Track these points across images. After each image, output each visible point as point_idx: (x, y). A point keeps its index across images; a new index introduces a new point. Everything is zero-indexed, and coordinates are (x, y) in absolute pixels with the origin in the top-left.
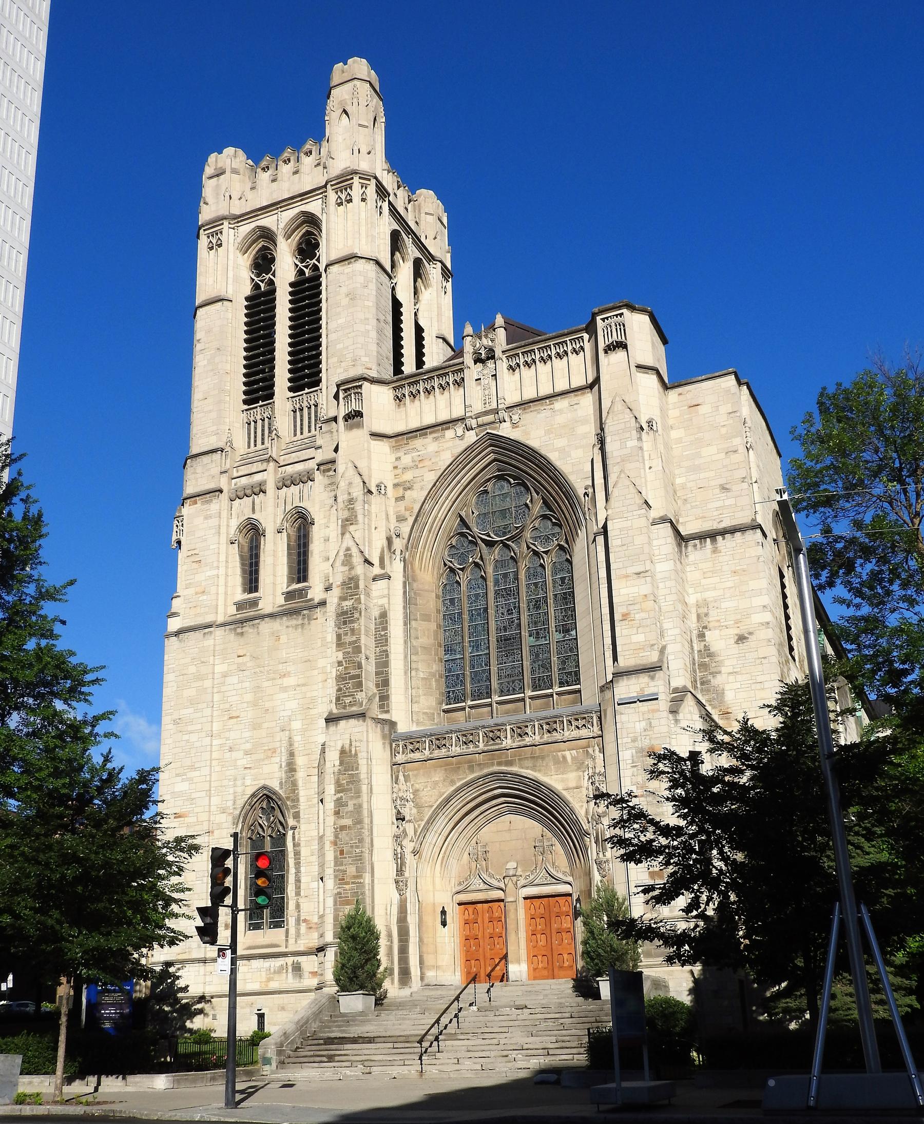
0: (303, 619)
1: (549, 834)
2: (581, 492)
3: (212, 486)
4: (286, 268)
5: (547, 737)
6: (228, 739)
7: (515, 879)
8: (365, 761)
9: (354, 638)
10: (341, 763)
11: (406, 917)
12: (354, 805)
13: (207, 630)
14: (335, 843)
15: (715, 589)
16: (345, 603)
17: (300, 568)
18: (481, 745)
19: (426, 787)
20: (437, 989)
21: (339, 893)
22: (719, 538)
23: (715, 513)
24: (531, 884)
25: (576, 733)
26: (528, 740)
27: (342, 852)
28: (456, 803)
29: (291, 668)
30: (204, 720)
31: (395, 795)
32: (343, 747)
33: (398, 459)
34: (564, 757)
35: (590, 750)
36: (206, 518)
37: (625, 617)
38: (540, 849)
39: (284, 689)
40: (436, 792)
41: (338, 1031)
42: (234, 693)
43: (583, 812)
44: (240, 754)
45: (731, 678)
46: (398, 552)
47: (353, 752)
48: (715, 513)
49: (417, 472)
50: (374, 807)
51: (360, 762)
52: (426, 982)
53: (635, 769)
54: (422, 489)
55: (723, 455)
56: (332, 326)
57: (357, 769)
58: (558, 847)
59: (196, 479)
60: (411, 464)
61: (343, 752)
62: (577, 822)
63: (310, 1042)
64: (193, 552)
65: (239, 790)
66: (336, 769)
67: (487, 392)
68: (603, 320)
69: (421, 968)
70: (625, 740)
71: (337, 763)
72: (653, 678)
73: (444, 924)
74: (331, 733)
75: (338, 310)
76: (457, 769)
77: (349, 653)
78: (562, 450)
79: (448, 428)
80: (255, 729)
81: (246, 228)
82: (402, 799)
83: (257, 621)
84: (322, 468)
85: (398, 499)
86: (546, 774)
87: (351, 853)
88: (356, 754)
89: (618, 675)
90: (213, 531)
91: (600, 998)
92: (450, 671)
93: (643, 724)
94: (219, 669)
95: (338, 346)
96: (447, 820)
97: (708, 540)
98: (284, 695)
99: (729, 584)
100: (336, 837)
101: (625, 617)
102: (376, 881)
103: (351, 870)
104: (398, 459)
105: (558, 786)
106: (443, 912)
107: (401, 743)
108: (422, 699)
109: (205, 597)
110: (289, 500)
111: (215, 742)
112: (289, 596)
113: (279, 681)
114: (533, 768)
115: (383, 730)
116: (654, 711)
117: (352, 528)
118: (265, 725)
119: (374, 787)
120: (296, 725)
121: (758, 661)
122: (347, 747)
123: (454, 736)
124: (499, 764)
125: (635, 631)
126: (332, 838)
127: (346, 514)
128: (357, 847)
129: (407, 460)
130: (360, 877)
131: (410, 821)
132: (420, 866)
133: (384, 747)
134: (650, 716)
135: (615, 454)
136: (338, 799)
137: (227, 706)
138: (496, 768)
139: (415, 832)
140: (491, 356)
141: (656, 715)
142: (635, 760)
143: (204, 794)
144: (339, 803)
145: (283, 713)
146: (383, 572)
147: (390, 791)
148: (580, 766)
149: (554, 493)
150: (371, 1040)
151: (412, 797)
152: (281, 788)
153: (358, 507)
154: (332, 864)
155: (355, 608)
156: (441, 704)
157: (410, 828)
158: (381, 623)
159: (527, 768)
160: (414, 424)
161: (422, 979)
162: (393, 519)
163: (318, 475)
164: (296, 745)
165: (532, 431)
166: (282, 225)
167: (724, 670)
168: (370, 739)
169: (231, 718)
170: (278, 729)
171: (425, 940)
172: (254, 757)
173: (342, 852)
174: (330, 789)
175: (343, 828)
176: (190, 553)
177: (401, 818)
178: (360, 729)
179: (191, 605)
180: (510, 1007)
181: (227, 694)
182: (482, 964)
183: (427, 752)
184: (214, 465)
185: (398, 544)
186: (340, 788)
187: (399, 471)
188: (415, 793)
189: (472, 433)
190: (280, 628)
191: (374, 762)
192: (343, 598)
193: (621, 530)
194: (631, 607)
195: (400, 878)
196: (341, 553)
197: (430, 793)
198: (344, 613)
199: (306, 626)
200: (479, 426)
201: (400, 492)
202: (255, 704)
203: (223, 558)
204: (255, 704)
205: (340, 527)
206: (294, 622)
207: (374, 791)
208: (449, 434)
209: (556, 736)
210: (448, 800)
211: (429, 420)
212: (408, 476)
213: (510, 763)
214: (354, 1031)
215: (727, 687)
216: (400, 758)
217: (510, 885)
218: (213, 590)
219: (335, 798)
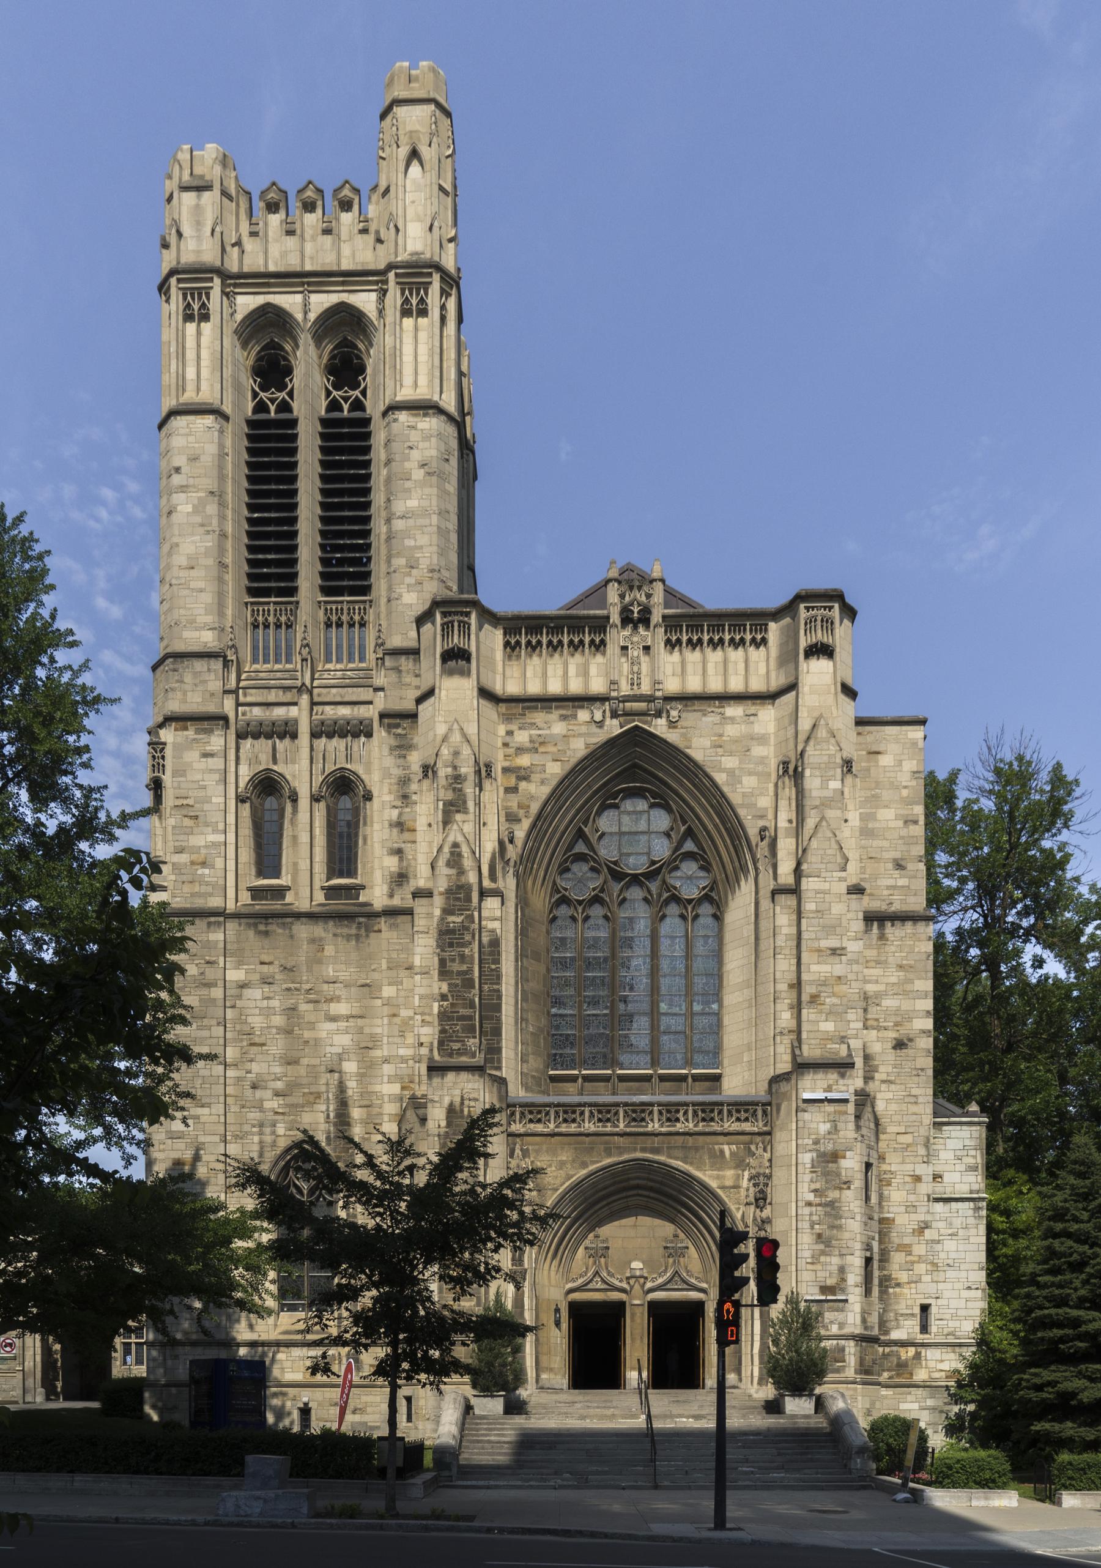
0: (359, 928)
1: (682, 1235)
2: (753, 832)
3: (211, 708)
4: (309, 390)
6: (249, 1072)
9: (464, 967)
10: (448, 1125)
13: (212, 919)
15: (877, 982)
16: (451, 919)
17: (343, 852)
18: (622, 1125)
22: (888, 924)
23: (886, 892)
25: (736, 1127)
26: (679, 1127)
29: (338, 990)
30: (215, 1041)
32: (451, 1104)
33: (510, 733)
34: (722, 1152)
35: (753, 1147)
36: (206, 755)
37: (814, 999)
39: (334, 1019)
42: (257, 1011)
43: (739, 1215)
44: (268, 1094)
45: (884, 1087)
46: (512, 863)
48: (886, 892)
49: (537, 759)
54: (542, 782)
55: (900, 823)
56: (399, 507)
59: (185, 693)
60: (528, 745)
64: (185, 802)
65: (268, 1139)
66: (443, 1131)
67: (635, 669)
68: (807, 609)
70: (806, 1141)
71: (443, 1123)
75: (408, 484)
76: (590, 1150)
77: (457, 985)
78: (731, 772)
79: (582, 707)
80: (289, 1064)
81: (247, 303)
83: (289, 920)
84: (386, 721)
85: (508, 790)
86: (698, 1168)
89: (801, 1067)
90: (217, 777)
93: (828, 1126)
94: (235, 975)
95: (410, 543)
97: (875, 924)
98: (333, 1026)
99: (893, 980)
101: (814, 999)
104: (510, 733)
105: (713, 1184)
106: (557, 1310)
108: (531, 1058)
109: (207, 871)
110: (330, 757)
111: (230, 1073)
112: (332, 892)
113: (325, 1007)
117: (458, 817)
118: (305, 1061)
120: (350, 1067)
122: (458, 1100)
124: (643, 1150)
125: (824, 1017)
127: (450, 796)
129: (522, 737)
135: (815, 794)
137: (246, 1028)
140: (644, 619)
141: (843, 1118)
143: (217, 1139)
145: (328, 1049)
146: (493, 886)
148: (740, 1164)
149: (710, 827)
152: (329, 1144)
153: (469, 789)
155: (467, 929)
158: (491, 953)
159: (677, 1159)
160: (534, 688)
161: (537, 1381)
162: (503, 819)
163: (380, 734)
164: (350, 1092)
165: (697, 737)
166: (312, 316)
167: (877, 1076)
169: (252, 1044)
170: (323, 1068)
172: (290, 1100)
176: (179, 802)
178: (476, 1086)
179: (184, 878)
181: (249, 1012)
183: (552, 1126)
184: (212, 676)
185: (512, 853)
187: (511, 751)
189: (615, 722)
190: (323, 935)
192: (447, 911)
193: (817, 892)
194: (823, 988)
196: (446, 849)
198: (451, 932)
199: (362, 939)
200: (626, 714)
201: (512, 782)
202: (288, 1032)
203: (231, 819)
204: (288, 1032)
205: (440, 813)
206: (345, 931)
208: (583, 715)
209: (715, 1127)
211: (555, 687)
212: (524, 761)
213: (656, 1151)
215: (878, 1096)
217: (637, 1287)
218: (219, 863)
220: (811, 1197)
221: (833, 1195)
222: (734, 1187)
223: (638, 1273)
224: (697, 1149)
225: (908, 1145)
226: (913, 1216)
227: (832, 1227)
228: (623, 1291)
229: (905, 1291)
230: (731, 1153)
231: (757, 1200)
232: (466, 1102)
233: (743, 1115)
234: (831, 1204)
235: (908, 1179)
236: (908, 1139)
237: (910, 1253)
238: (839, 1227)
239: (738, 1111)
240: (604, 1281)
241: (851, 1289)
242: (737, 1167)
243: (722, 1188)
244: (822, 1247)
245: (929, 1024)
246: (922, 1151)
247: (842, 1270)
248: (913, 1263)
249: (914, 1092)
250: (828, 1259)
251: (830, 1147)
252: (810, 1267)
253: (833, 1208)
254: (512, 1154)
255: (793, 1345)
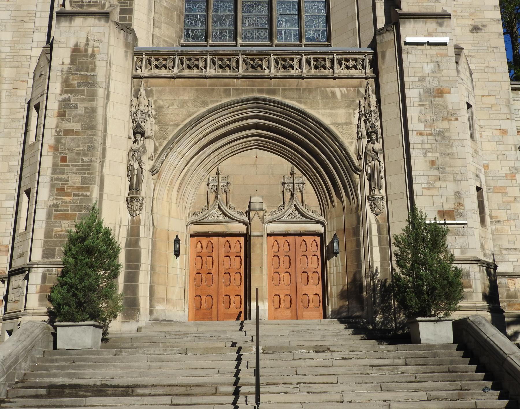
5: (313, 72)
7: (261, 213)
8: (104, 64)
10: (72, 62)
11: (137, 242)
12: (86, 108)
14: (55, 148)
18: (241, 70)
19: (173, 104)
20: (165, 325)
21: (56, 205)
24: (278, 221)
26: (293, 72)
27: (64, 159)
28: (207, 126)
31: (133, 109)
32: (76, 45)
34: (333, 94)
38: (290, 188)
40: (184, 111)
41: (65, 375)
47: (90, 51)
50: (109, 115)
51: (98, 63)
52: (155, 315)
53: (423, 108)
57: (93, 70)
58: (308, 187)
61: (76, 50)
62: (348, 156)
63: (22, 392)
66: (65, 68)
69: (151, 300)
71: (68, 61)
72: (441, 25)
73: (177, 254)
74: (61, 28)
76: (211, 90)
82: (143, 113)
86: (312, 107)
87: (75, 160)
88: (93, 55)
91: (418, 341)
92: (190, 10)
96: (193, 142)
100: (58, 140)
102: (105, 197)
103: (75, 180)
105: (327, 121)
106: (177, 241)
107: (145, 58)
114: (299, 100)
115: (126, 39)
116: (442, 55)
119: (112, 95)
121: (490, 50)
123: (209, 58)
124: (260, 91)
126: (52, 142)
128: (85, 155)
130: (87, 189)
131: (150, 137)
132: (158, 186)
133: (126, 56)
134: (439, 59)
136: (64, 100)
138: (256, 95)
139: (155, 150)
142: (423, 98)
144: (65, 105)
147: (129, 103)
150: (128, 391)
151: (154, 113)
154: (50, 171)
156: (180, 38)
157: (150, 145)
159: (292, 99)
161: (151, 312)
168: (112, 43)
171: (157, 269)
173: (64, 159)
174: (56, 88)
175: (67, 132)
177: (138, 132)
180: (308, 348)
182: (215, 300)
186: (67, 87)
188: (159, 109)
191: (113, 67)
195: (135, 197)
197: (177, 112)
207: (111, 98)
210: (198, 120)
214: (91, 376)
216: (144, 72)
219: (61, 98)
220: (421, 127)
221: (442, 125)
222: (347, 124)
223: (257, 207)
224: (310, 91)
225: (492, 105)
226: (504, 163)
227: (444, 154)
228: (245, 223)
229: (506, 227)
230: (342, 95)
231: (369, 135)
232: (91, 43)
233: (352, 63)
234: (441, 133)
235: (496, 132)
236: (491, 100)
237: (505, 194)
238: (451, 155)
239: (347, 60)
240: (225, 215)
241: (468, 214)
242: (348, 106)
243: (336, 124)
244: (436, 173)
245: (498, 15)
246: (505, 110)
247: (458, 194)
248: (509, 203)
249: (492, 64)
250: (443, 184)
251: (434, 84)
252: (426, 192)
253: (444, 138)
254: (137, 94)
255: (419, 262)
